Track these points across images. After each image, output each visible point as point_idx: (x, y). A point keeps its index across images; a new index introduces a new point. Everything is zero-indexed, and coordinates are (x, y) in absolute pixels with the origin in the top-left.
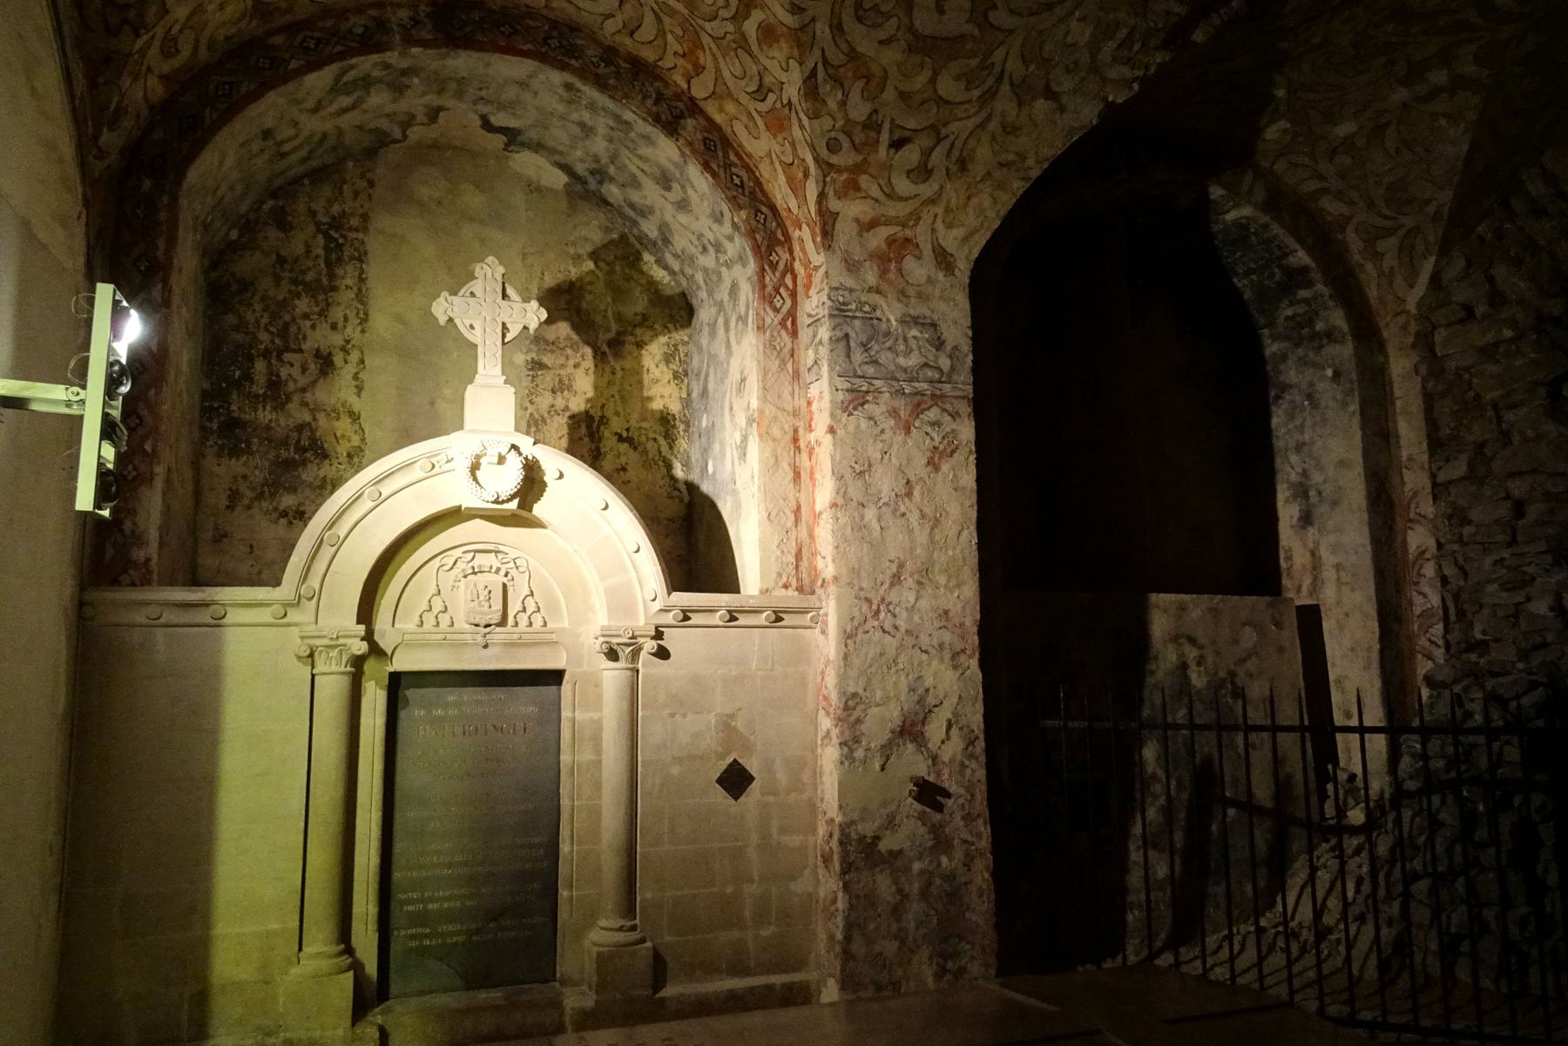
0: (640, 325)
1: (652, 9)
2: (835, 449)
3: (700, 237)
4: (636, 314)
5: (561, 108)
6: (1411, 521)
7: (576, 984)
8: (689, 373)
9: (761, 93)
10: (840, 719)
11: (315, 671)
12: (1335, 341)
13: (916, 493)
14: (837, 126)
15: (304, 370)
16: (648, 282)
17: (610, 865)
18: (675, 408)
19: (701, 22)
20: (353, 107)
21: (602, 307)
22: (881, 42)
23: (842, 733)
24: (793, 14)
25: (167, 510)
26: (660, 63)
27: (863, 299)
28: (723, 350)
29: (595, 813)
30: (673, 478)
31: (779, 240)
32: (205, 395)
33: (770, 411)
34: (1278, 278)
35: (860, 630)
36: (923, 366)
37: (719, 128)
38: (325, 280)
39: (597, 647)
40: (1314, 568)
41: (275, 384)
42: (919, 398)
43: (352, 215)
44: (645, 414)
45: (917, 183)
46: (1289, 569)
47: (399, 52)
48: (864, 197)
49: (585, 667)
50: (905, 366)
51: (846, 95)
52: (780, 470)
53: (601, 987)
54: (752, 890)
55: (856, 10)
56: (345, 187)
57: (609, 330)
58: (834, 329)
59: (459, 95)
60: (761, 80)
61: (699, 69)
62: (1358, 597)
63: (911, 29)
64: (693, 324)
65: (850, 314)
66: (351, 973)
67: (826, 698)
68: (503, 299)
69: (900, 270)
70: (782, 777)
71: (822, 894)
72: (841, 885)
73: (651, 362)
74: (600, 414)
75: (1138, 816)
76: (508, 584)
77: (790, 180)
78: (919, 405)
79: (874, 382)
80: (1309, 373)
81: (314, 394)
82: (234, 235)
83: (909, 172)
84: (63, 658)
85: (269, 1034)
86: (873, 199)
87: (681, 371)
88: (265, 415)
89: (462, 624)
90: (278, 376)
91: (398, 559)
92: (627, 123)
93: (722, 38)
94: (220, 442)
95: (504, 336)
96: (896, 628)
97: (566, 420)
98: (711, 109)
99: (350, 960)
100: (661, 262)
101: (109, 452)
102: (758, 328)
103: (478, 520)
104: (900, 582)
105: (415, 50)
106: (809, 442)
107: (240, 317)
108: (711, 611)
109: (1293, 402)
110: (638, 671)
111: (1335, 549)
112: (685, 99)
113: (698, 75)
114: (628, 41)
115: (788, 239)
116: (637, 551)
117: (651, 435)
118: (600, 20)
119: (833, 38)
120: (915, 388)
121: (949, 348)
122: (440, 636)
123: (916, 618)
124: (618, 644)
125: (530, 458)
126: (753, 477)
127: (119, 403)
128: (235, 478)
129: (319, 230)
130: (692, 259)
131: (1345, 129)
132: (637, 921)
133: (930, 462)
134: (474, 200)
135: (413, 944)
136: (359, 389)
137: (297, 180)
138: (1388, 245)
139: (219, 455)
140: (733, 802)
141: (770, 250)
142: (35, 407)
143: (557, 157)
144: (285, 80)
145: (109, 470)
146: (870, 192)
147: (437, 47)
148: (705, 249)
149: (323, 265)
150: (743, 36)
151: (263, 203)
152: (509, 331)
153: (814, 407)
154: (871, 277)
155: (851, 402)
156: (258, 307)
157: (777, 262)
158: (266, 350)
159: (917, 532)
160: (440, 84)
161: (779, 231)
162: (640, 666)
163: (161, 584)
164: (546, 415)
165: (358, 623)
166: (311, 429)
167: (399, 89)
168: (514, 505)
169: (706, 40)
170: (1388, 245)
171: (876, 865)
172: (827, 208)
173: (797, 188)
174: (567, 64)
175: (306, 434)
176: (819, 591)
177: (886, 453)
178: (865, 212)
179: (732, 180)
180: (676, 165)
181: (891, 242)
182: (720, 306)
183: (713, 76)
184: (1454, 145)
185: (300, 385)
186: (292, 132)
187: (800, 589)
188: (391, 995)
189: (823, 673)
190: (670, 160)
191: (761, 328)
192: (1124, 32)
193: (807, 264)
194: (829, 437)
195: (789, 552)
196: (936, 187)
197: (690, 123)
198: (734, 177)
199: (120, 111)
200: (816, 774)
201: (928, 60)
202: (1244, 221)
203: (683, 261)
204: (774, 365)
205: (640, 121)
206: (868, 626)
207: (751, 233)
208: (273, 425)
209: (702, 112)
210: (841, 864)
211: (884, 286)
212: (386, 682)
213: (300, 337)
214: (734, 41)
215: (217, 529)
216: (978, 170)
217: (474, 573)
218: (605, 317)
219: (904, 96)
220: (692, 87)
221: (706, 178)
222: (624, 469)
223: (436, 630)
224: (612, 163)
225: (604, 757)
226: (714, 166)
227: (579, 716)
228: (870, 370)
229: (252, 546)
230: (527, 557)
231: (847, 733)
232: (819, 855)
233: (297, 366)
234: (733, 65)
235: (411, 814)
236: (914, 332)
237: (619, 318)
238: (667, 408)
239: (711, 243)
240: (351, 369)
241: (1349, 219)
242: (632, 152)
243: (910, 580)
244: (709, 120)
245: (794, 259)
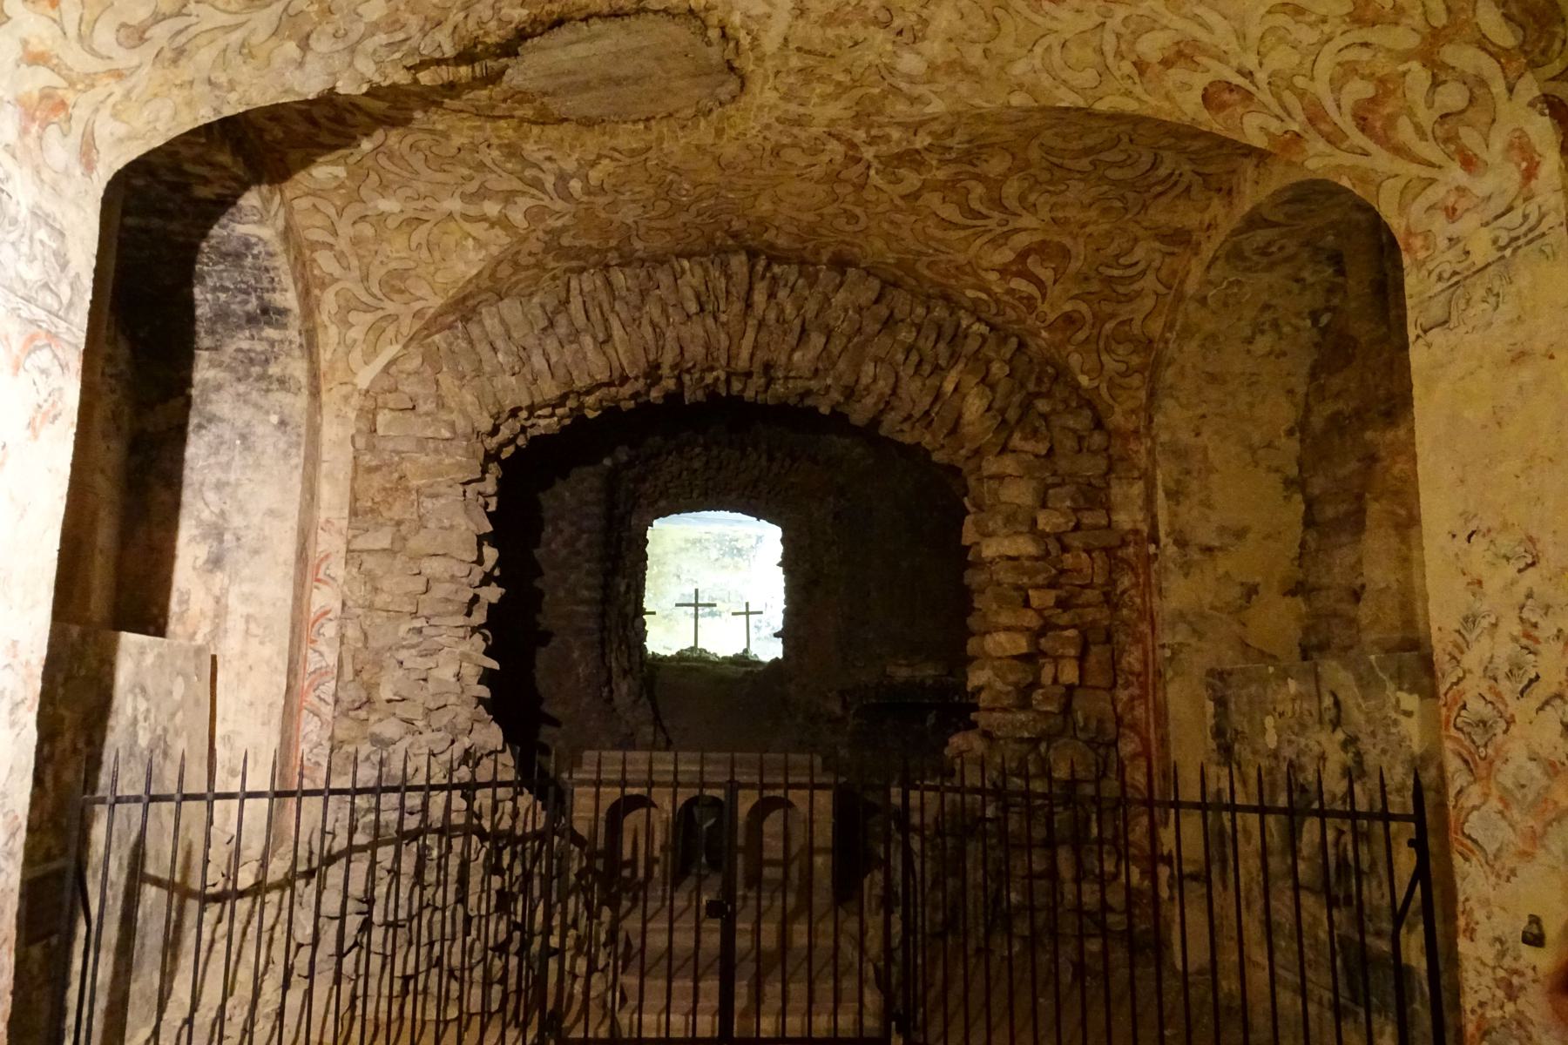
6: (318, 580)
12: (288, 391)
40: (216, 616)
45: (120, 44)
46: (182, 613)
48: (54, 21)
62: (268, 651)
69: (40, 138)
75: (82, 913)
80: (247, 413)
83: (124, 25)
109: (219, 436)
111: (246, 598)
121: (72, 273)
131: (388, 205)
133: (31, 425)
138: (362, 320)
170: (362, 320)
178: (42, 41)
181: (47, 95)
184: (466, 264)
192: (401, 36)
196: (135, 61)
202: (253, 240)
216: (186, 71)
241: (337, 280)
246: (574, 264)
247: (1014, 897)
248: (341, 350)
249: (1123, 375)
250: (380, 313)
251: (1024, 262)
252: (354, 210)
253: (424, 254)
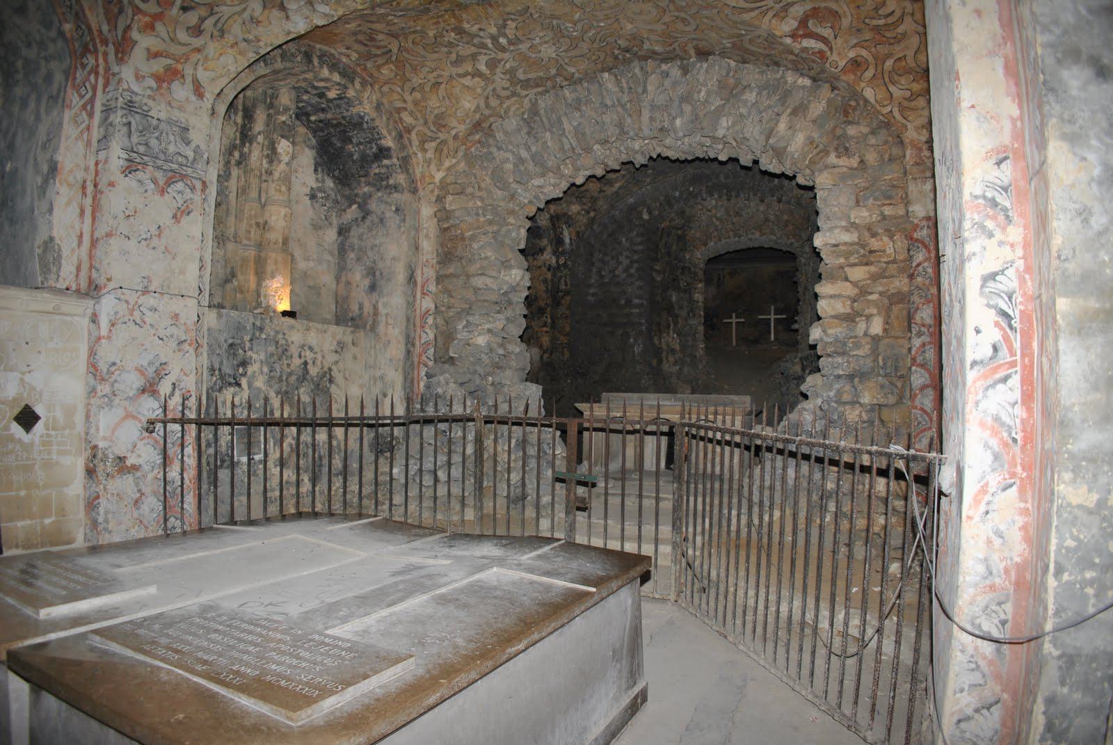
34: (374, 150)
78: (171, 178)
79: (145, 158)
80: (383, 206)
115: (96, 51)
133: (175, 217)
155: (127, 167)
181: (168, 69)
216: (230, 39)
228: (142, 149)
246: (540, 89)
248: (426, 165)
249: (909, 100)
250: (438, 141)
251: (807, 27)
252: (408, 86)
253: (447, 102)
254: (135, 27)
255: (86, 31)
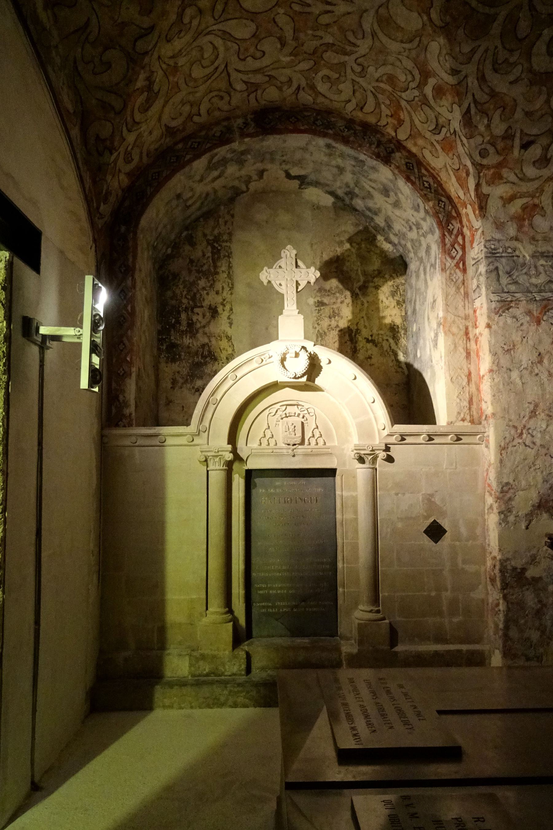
0: (376, 276)
1: (372, 92)
2: (491, 337)
3: (407, 221)
4: (374, 270)
5: (326, 159)
7: (348, 639)
8: (406, 300)
9: (437, 129)
10: (498, 498)
11: (208, 469)
13: (546, 361)
14: (485, 141)
15: (204, 316)
16: (381, 251)
17: (364, 576)
18: (398, 321)
19: (399, 94)
20: (219, 176)
21: (355, 268)
22: (511, 83)
23: (500, 506)
24: (453, 75)
25: (139, 390)
26: (379, 124)
27: (507, 245)
28: (423, 285)
29: (355, 547)
30: (398, 361)
31: (454, 216)
32: (159, 333)
33: (450, 317)
35: (510, 445)
36: (548, 282)
37: (414, 155)
38: (212, 270)
39: (353, 456)
41: (191, 324)
42: (545, 302)
43: (224, 234)
44: (381, 326)
45: (540, 169)
47: (239, 143)
49: (347, 467)
50: (536, 283)
51: (490, 120)
52: (458, 352)
53: (361, 642)
54: (447, 595)
55: (493, 65)
56: (220, 220)
57: (359, 281)
58: (489, 265)
59: (272, 160)
60: (437, 122)
61: (401, 122)
63: (530, 70)
64: (407, 273)
65: (498, 255)
66: (232, 623)
67: (489, 485)
68: (296, 267)
70: (463, 530)
71: (490, 601)
72: (501, 595)
73: (383, 296)
74: (356, 328)
76: (304, 422)
77: (458, 179)
78: (545, 306)
79: (516, 295)
81: (209, 328)
82: (169, 251)
83: (534, 163)
84: (94, 464)
85: (193, 650)
86: (512, 183)
87: (401, 300)
88: (187, 341)
89: (281, 444)
90: (192, 320)
91: (247, 411)
92: (361, 161)
93: (412, 101)
94: (167, 355)
95: (297, 288)
96: (534, 443)
97: (337, 332)
98: (409, 145)
99: (231, 617)
100: (388, 240)
101: (96, 360)
102: (442, 270)
103: (287, 389)
104: (535, 415)
105: (247, 140)
106: (476, 334)
107: (174, 292)
108: (418, 435)
110: (376, 469)
112: (394, 142)
113: (400, 126)
114: (360, 114)
115: (459, 215)
116: (374, 402)
117: (385, 338)
118: (343, 104)
119: (480, 86)
120: (543, 296)
122: (270, 451)
123: (547, 437)
124: (364, 454)
125: (312, 353)
126: (441, 357)
127: (100, 335)
128: (174, 373)
129: (208, 243)
130: (404, 235)
132: (380, 608)
134: (284, 218)
135: (264, 610)
136: (231, 324)
137: (197, 220)
139: (167, 363)
140: (434, 544)
141: (448, 222)
142: (65, 340)
143: (327, 188)
144: (183, 167)
145: (96, 368)
146: (509, 179)
147: (257, 136)
148: (411, 228)
149: (211, 261)
150: (425, 96)
151: (181, 233)
152: (299, 284)
153: (478, 312)
154: (512, 231)
155: (501, 308)
156: (181, 287)
157: (453, 230)
158: (186, 308)
159: (546, 385)
160: (261, 157)
161: (453, 211)
162: (377, 466)
163: (138, 425)
164: (326, 331)
165: (228, 444)
166: (208, 346)
167: (241, 163)
168: (304, 379)
169: (403, 103)
171: (524, 586)
172: (482, 192)
173: (463, 184)
174: (327, 133)
175: (207, 348)
176: (484, 422)
177: (524, 337)
178: (507, 192)
179: (424, 185)
180: (391, 181)
181: (524, 208)
182: (421, 260)
183: (409, 124)
185: (202, 325)
186: (190, 194)
187: (472, 422)
188: (254, 636)
189: (487, 470)
190: (387, 179)
191: (443, 270)
193: (471, 228)
194: (487, 330)
195: (465, 400)
197: (398, 155)
198: (425, 183)
199: (108, 193)
200: (485, 530)
201: (544, 89)
203: (400, 237)
204: (452, 290)
205: (369, 159)
206: (515, 443)
207: (436, 215)
208: (191, 345)
209: (405, 148)
210: (501, 584)
211: (520, 236)
212: (244, 474)
213: (202, 299)
214: (419, 101)
215: (167, 398)
217: (287, 417)
218: (357, 274)
219: (528, 114)
220: (398, 134)
221: (408, 186)
222: (370, 358)
223: (268, 447)
224: (356, 186)
225: (359, 517)
226: (412, 178)
227: (345, 494)
228: (513, 288)
229: (183, 407)
230: (314, 407)
231: (503, 507)
232: (488, 577)
233: (201, 314)
234: (420, 115)
235: (259, 544)
236: (542, 262)
237: (365, 273)
238: (394, 322)
239: (414, 224)
240: (226, 314)
242: (366, 178)
243: (543, 415)
244: (409, 152)
245: (463, 226)
247: (290, 128)
254: (484, 184)
255: (447, 202)
